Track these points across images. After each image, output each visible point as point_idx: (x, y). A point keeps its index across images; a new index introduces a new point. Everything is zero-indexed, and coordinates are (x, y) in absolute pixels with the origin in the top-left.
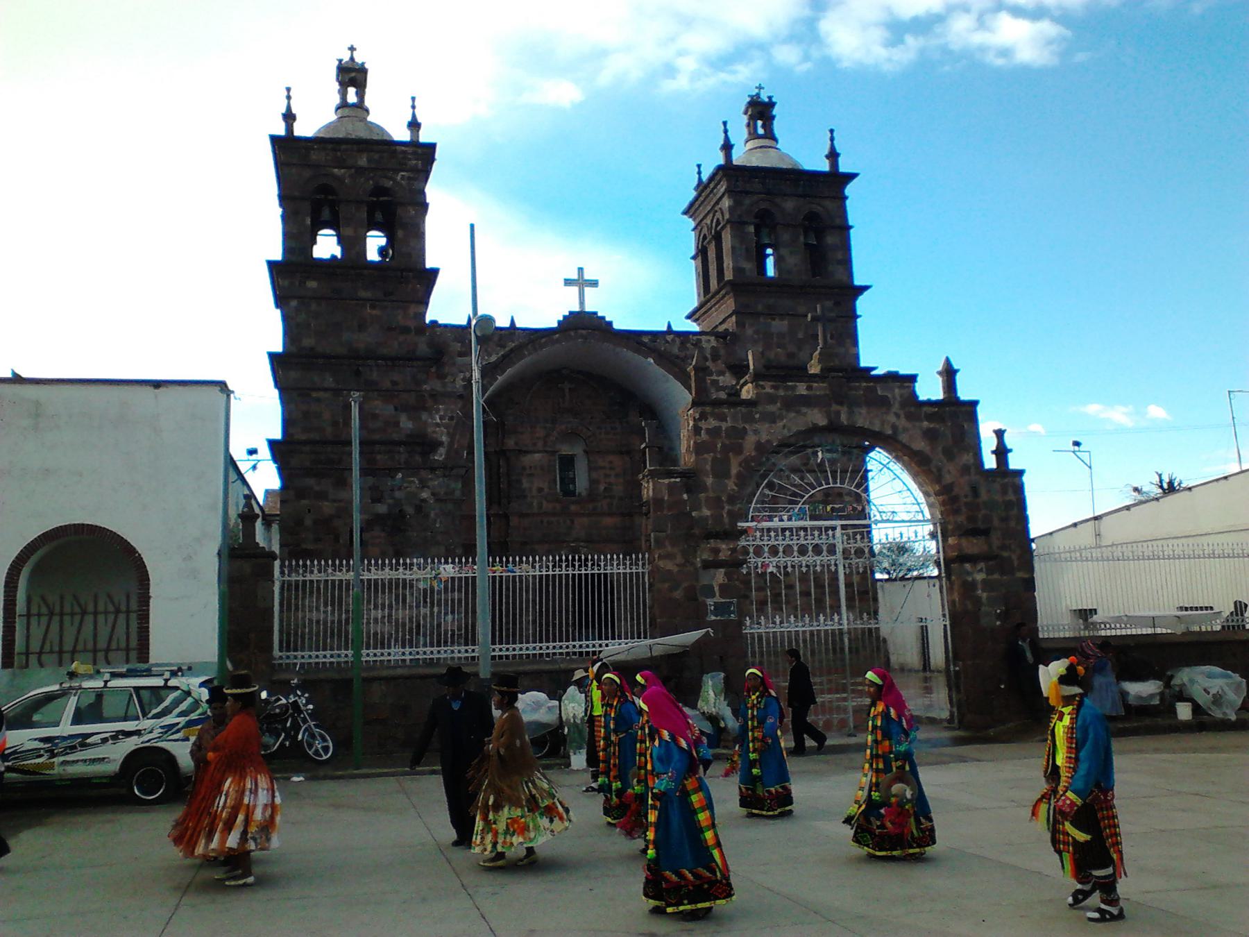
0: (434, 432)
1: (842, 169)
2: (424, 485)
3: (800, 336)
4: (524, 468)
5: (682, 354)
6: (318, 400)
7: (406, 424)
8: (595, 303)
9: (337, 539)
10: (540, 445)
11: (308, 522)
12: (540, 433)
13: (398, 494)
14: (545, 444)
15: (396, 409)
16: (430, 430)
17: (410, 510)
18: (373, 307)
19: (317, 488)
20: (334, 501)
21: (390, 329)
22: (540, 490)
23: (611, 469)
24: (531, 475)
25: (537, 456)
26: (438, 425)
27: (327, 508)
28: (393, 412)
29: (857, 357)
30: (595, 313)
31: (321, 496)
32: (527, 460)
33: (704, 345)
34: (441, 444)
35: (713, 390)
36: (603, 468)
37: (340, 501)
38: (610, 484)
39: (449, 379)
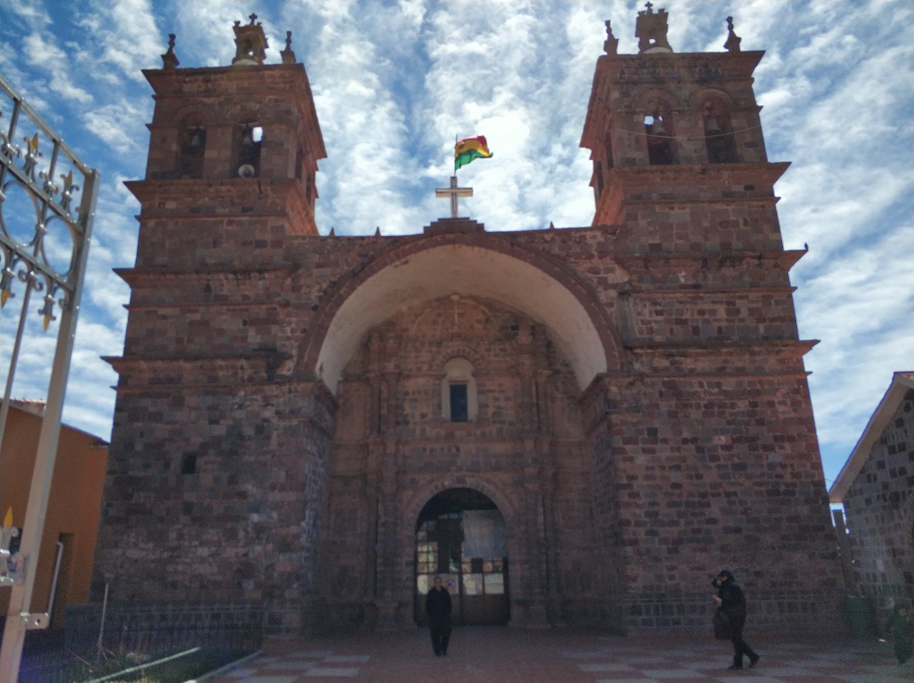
0: (283, 346)
1: (744, 47)
2: (267, 403)
3: (706, 224)
4: (407, 394)
5: (564, 253)
6: (164, 317)
7: (254, 338)
8: (467, 209)
9: (167, 465)
10: (425, 368)
11: (139, 447)
12: (425, 356)
13: (239, 414)
14: (430, 368)
15: (245, 323)
16: (278, 344)
17: (249, 431)
18: (230, 223)
19: (151, 409)
20: (169, 423)
21: (245, 243)
22: (423, 416)
23: (502, 392)
24: (416, 400)
25: (421, 381)
26: (289, 338)
27: (160, 431)
28: (241, 326)
29: (780, 242)
30: (468, 218)
31: (157, 417)
32: (411, 385)
33: (590, 241)
34: (291, 357)
35: (600, 289)
36: (493, 391)
37: (176, 423)
38: (499, 407)
39: (304, 290)
